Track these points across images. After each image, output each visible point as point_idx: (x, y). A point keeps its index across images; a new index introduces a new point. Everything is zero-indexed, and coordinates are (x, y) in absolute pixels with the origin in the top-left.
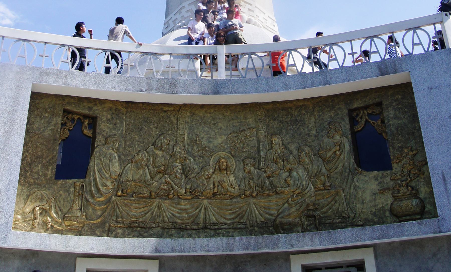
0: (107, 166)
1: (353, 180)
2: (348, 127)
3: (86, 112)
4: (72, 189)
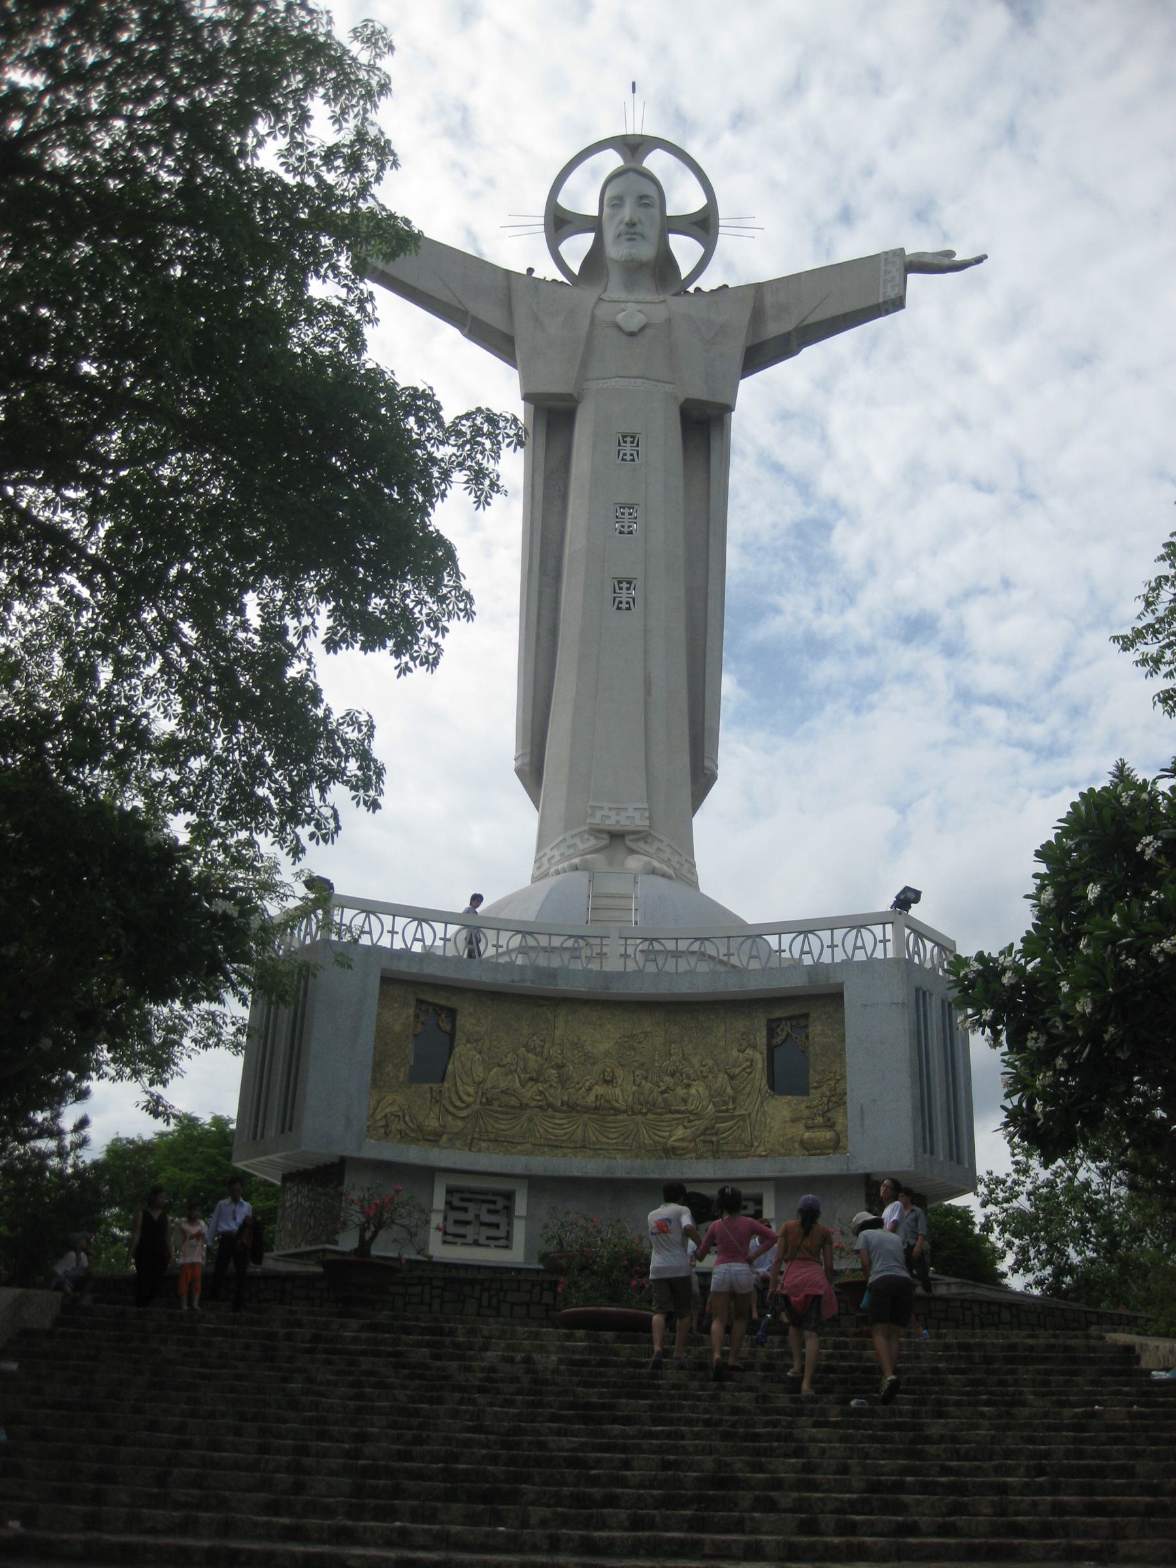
2: (765, 1040)
3: (443, 1002)
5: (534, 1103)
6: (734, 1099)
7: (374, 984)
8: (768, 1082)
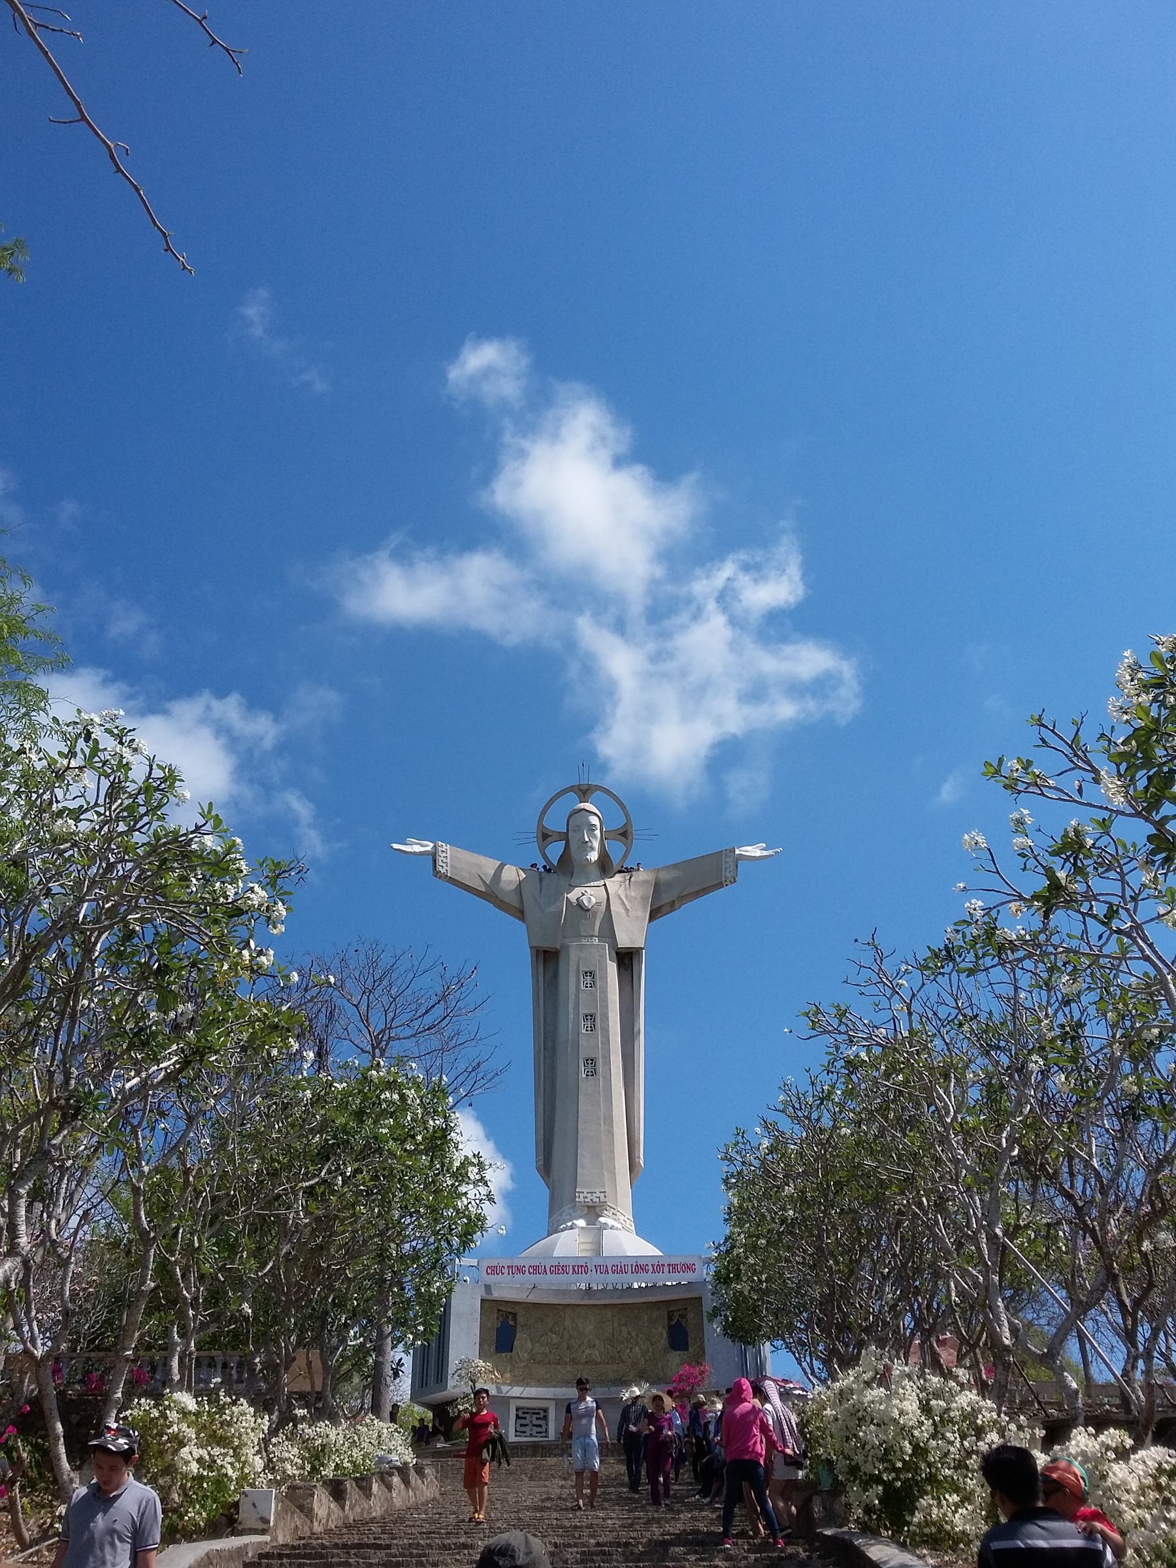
0: (522, 1341)
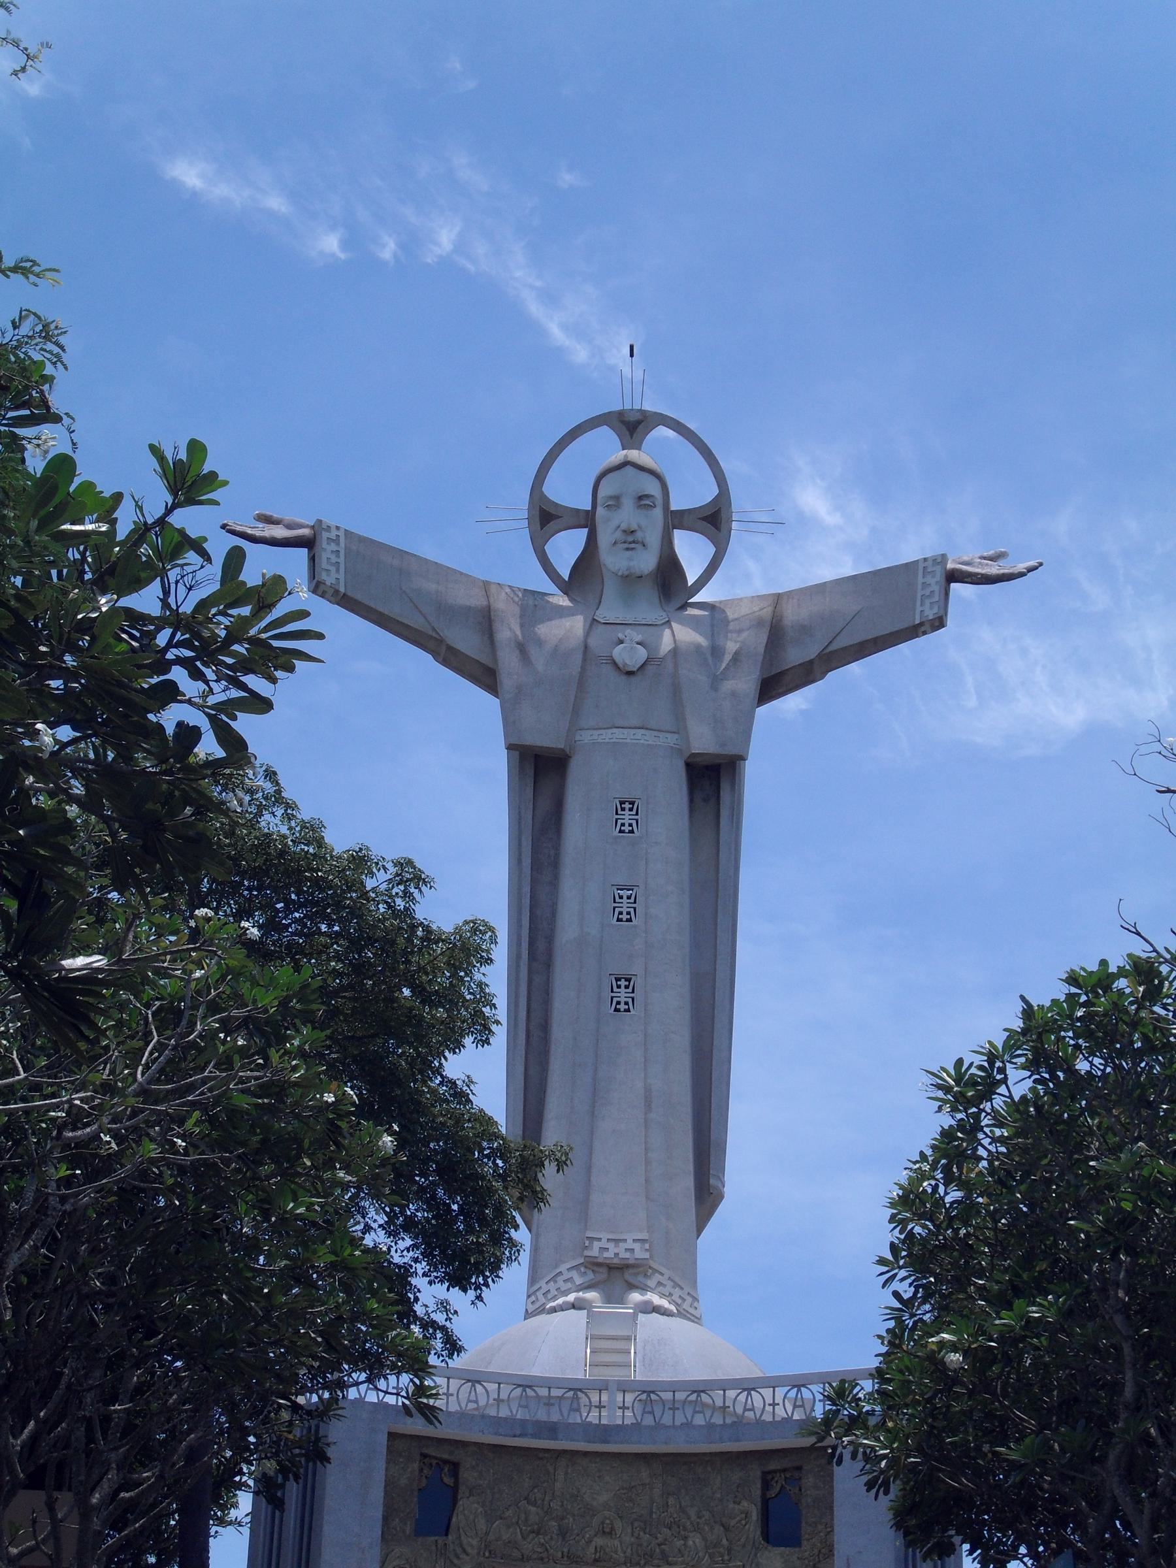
1: (756, 1555)
2: (759, 1492)
3: (446, 1456)
4: (434, 1548)
5: (535, 1556)
6: (729, 1551)
7: (383, 1439)
8: (762, 1533)
